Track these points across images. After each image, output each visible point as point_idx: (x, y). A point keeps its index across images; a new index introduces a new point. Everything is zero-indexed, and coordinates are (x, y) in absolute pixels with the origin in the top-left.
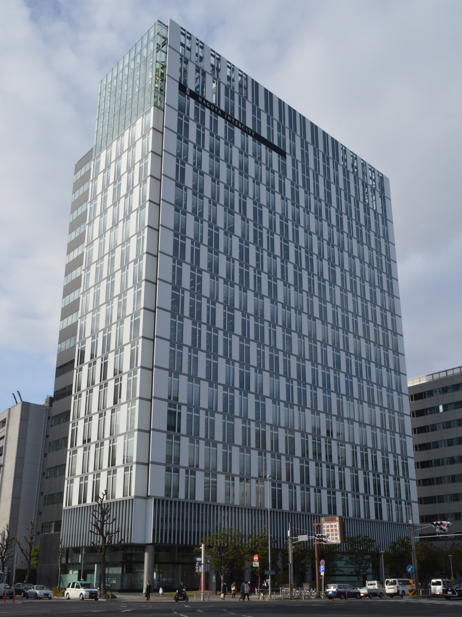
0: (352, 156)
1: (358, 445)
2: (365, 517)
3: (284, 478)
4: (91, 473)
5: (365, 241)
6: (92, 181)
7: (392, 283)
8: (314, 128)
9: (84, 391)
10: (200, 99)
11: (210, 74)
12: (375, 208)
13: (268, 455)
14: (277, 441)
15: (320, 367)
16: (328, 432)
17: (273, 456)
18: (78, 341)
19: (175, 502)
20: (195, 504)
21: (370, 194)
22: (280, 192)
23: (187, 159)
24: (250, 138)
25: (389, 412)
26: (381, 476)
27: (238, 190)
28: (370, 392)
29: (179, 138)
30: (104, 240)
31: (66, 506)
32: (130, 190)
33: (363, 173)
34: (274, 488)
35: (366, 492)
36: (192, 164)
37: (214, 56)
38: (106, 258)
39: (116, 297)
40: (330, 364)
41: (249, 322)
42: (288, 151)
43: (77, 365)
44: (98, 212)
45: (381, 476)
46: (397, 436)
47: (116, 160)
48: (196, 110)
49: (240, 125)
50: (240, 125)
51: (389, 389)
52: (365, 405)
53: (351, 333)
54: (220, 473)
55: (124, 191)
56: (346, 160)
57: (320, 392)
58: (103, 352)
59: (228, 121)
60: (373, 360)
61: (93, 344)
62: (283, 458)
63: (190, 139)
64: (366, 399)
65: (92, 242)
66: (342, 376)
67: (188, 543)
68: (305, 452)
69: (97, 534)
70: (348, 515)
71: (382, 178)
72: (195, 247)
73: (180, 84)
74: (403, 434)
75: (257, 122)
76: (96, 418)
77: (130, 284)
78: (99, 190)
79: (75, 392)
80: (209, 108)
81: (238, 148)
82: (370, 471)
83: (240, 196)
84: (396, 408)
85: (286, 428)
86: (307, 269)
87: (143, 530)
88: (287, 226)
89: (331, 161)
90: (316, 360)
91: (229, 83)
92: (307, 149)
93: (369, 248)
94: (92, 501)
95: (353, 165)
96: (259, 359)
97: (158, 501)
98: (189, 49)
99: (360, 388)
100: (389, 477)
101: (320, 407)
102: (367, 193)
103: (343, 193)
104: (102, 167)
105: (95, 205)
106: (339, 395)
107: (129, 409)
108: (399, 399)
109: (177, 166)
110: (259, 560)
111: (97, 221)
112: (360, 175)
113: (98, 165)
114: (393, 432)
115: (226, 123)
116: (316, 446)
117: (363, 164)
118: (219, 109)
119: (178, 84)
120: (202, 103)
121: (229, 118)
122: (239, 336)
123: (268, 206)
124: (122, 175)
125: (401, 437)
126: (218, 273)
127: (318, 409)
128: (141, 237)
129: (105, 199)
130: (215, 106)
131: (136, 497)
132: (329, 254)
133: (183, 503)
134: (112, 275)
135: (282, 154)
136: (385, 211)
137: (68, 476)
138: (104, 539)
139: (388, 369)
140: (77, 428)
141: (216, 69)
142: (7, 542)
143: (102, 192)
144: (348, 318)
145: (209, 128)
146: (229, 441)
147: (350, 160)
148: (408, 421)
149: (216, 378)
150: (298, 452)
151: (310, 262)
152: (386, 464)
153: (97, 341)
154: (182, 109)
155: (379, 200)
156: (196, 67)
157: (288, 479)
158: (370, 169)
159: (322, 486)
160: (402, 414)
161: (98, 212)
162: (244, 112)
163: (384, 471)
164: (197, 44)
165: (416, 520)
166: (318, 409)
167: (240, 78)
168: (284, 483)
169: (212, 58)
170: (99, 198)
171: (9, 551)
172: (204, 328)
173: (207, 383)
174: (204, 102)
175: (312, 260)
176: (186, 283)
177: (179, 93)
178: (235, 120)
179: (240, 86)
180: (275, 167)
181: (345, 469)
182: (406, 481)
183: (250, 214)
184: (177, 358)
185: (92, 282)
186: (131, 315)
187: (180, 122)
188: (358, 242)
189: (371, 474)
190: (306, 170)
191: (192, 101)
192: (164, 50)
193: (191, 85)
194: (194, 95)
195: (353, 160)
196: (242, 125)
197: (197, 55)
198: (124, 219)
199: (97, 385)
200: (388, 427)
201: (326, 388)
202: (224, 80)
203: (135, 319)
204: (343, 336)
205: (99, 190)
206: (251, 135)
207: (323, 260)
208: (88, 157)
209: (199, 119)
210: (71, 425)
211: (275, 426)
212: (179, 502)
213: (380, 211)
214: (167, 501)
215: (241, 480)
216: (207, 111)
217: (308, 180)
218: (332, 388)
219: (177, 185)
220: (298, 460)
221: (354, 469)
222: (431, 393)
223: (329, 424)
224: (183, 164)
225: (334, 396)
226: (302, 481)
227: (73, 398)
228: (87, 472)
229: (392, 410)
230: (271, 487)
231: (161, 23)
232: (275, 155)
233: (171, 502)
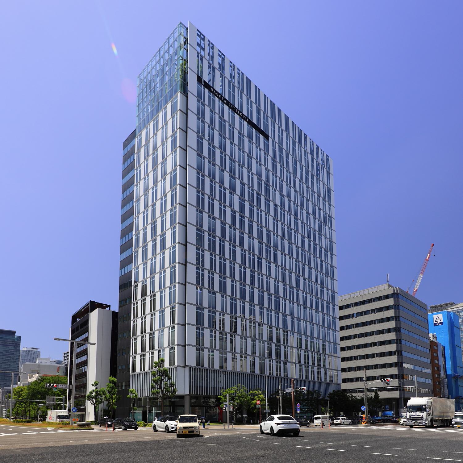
2: (209, 366)
3: (266, 356)
4: (147, 352)
5: (316, 204)
6: (137, 153)
9: (139, 300)
11: (218, 70)
12: (323, 181)
13: (257, 341)
14: (262, 334)
17: (260, 342)
18: (133, 267)
19: (202, 369)
20: (214, 371)
22: (266, 226)
23: (204, 136)
24: (245, 123)
27: (238, 161)
29: (198, 119)
31: (132, 372)
32: (165, 158)
34: (260, 361)
36: (207, 139)
42: (270, 135)
43: (134, 283)
45: (320, 300)
46: (331, 331)
48: (209, 98)
49: (239, 113)
50: (239, 113)
53: (306, 265)
54: (228, 352)
55: (160, 159)
58: (151, 274)
59: (231, 108)
60: (321, 338)
62: (266, 343)
63: (206, 120)
66: (301, 293)
68: (278, 340)
70: (302, 378)
73: (198, 76)
78: (142, 159)
79: (134, 301)
80: (218, 97)
81: (238, 196)
82: (316, 352)
83: (240, 233)
86: (282, 281)
87: (183, 387)
88: (270, 251)
94: (149, 369)
96: (251, 280)
97: (191, 369)
103: (304, 168)
104: (143, 142)
105: (140, 171)
109: (198, 140)
113: (140, 141)
114: (329, 328)
115: (229, 110)
118: (225, 99)
119: (196, 75)
120: (213, 92)
121: (232, 106)
123: (257, 174)
124: (158, 148)
125: (333, 332)
126: (226, 293)
128: (175, 192)
130: (222, 96)
131: (178, 366)
132: (295, 212)
133: (207, 370)
135: (266, 136)
137: (132, 354)
139: (330, 342)
140: (136, 324)
141: (222, 67)
145: (218, 113)
151: (283, 215)
154: (200, 96)
156: (208, 63)
157: (267, 290)
163: (323, 352)
173: (220, 295)
174: (215, 92)
175: (284, 214)
176: (205, 153)
177: (197, 83)
183: (246, 180)
184: (201, 259)
187: (198, 178)
189: (316, 354)
190: (281, 150)
191: (206, 90)
192: (186, 48)
193: (206, 78)
194: (207, 86)
196: (240, 112)
199: (148, 296)
200: (326, 326)
203: (173, 250)
205: (142, 159)
206: (246, 121)
207: (291, 215)
208: (133, 135)
209: (212, 104)
210: (132, 322)
212: (205, 370)
214: (197, 369)
216: (217, 99)
219: (198, 154)
220: (304, 351)
224: (201, 139)
227: (132, 305)
231: (183, 25)
232: (261, 137)
233: (200, 369)
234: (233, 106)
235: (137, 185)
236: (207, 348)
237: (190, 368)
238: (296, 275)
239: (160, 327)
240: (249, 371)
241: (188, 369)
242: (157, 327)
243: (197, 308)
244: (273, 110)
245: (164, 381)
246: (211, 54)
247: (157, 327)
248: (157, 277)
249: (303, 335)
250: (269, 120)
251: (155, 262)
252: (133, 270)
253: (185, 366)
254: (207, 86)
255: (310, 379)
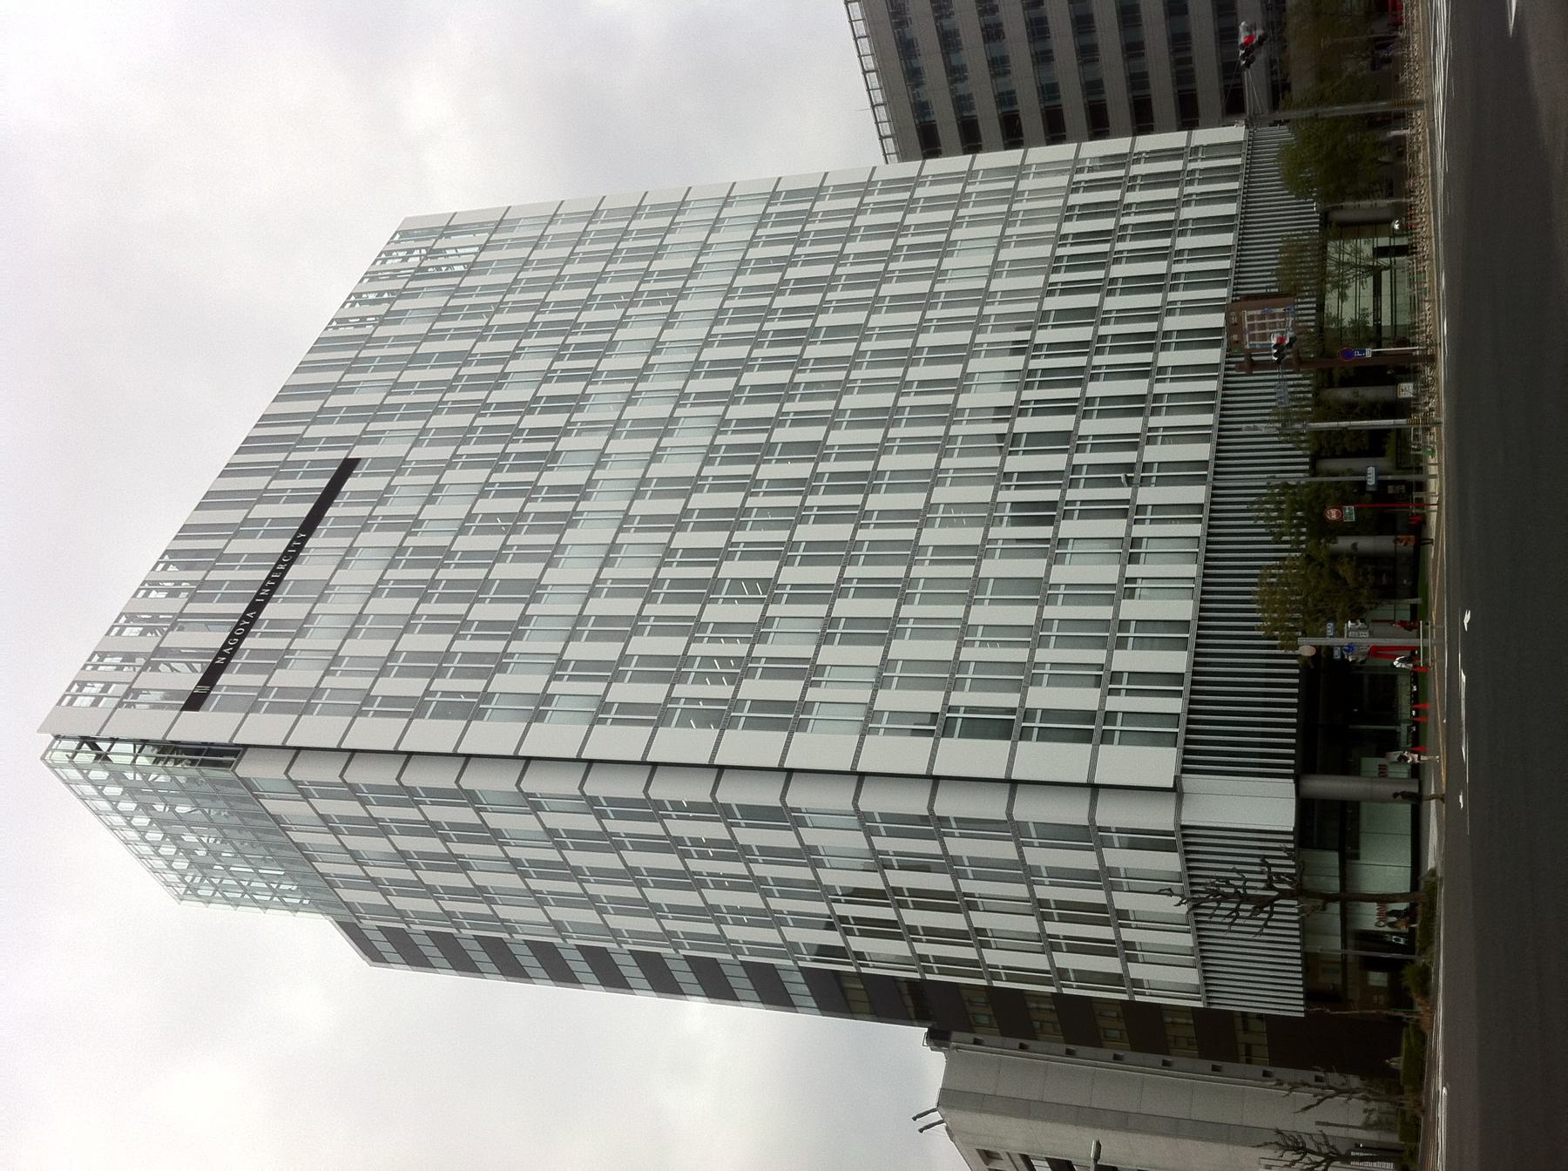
0: (353, 303)
1: (1047, 278)
2: (1214, 377)
7: (652, 206)
8: (212, 500)
10: (221, 660)
15: (854, 374)
16: (1015, 352)
17: (1073, 484)
21: (441, 261)
25: (966, 205)
26: (1125, 220)
28: (916, 251)
30: (549, 893)
33: (393, 277)
35: (1164, 257)
37: (123, 628)
38: (593, 889)
39: (685, 865)
40: (847, 349)
41: (747, 544)
42: (341, 455)
44: (483, 909)
47: (361, 865)
49: (282, 567)
50: (282, 567)
51: (908, 207)
52: (947, 263)
54: (1116, 612)
56: (363, 319)
57: (876, 502)
61: (798, 924)
64: (934, 262)
65: (553, 923)
67: (1296, 690)
69: (1272, 913)
71: (404, 234)
72: (569, 672)
73: (186, 707)
74: (1019, 172)
75: (273, 528)
76: (979, 919)
77: (654, 828)
78: (428, 905)
80: (241, 638)
84: (956, 188)
85: (970, 603)
87: (1264, 806)
89: (294, 456)
90: (836, 383)
91: (183, 595)
92: (337, 409)
93: (515, 355)
95: (373, 302)
98: (108, 685)
99: (906, 276)
100: (1126, 202)
101: (954, 371)
102: (438, 268)
104: (375, 898)
105: (467, 916)
106: (884, 448)
107: (957, 832)
108: (933, 183)
110: (1340, 504)
111: (503, 912)
112: (398, 284)
116: (1051, 378)
117: (372, 279)
118: (244, 617)
120: (229, 657)
121: (265, 592)
122: (780, 568)
127: (921, 507)
129: (455, 893)
130: (238, 626)
134: (631, 875)
135: (348, 467)
136: (481, 224)
138: (1283, 894)
140: (1004, 968)
141: (151, 623)
142: (1286, 1148)
143: (436, 899)
144: (779, 214)
146: (1039, 591)
147: (360, 310)
148: (988, 160)
149: (884, 621)
150: (1064, 423)
152: (1068, 317)
153: (790, 913)
155: (456, 240)
157: (1134, 446)
158: (384, 261)
159: (1127, 501)
160: (970, 175)
161: (483, 909)
162: (252, 556)
164: (95, 667)
165: (1236, 133)
166: (921, 507)
167: (171, 568)
168: (1140, 456)
169: (127, 632)
170: (449, 906)
171: (1311, 1146)
172: (811, 500)
178: (269, 578)
179: (189, 567)
180: (379, 483)
181: (1105, 308)
182: (1137, 161)
185: (650, 925)
186: (729, 826)
188: (499, 386)
193: (189, 681)
194: (211, 675)
195: (361, 303)
196: (280, 562)
197: (120, 668)
198: (501, 845)
201: (867, 483)
202: (176, 605)
204: (680, 564)
206: (304, 540)
211: (964, 632)
213: (482, 238)
215: (1133, 559)
217: (410, 405)
218: (867, 466)
220: (1108, 299)
221: (1108, 287)
222: (921, 109)
223: (994, 350)
225: (888, 462)
226: (1138, 412)
228: (1112, 942)
229: (961, 200)
230: (1153, 488)
232: (351, 485)
234: (263, 587)
235: (511, 930)
236: (1103, 701)
237: (1184, 771)
238: (1011, 453)
239: (1105, 923)
240: (1196, 530)
241: (1190, 781)
242: (1106, 933)
243: (947, 731)
244: (267, 444)
245: (1240, 883)
246: (117, 660)
247: (1106, 933)
248: (912, 917)
249: (1041, 305)
250: (294, 456)
251: (858, 920)
252: (801, 964)
253: (1176, 790)
254: (211, 675)
255: (1226, 264)
